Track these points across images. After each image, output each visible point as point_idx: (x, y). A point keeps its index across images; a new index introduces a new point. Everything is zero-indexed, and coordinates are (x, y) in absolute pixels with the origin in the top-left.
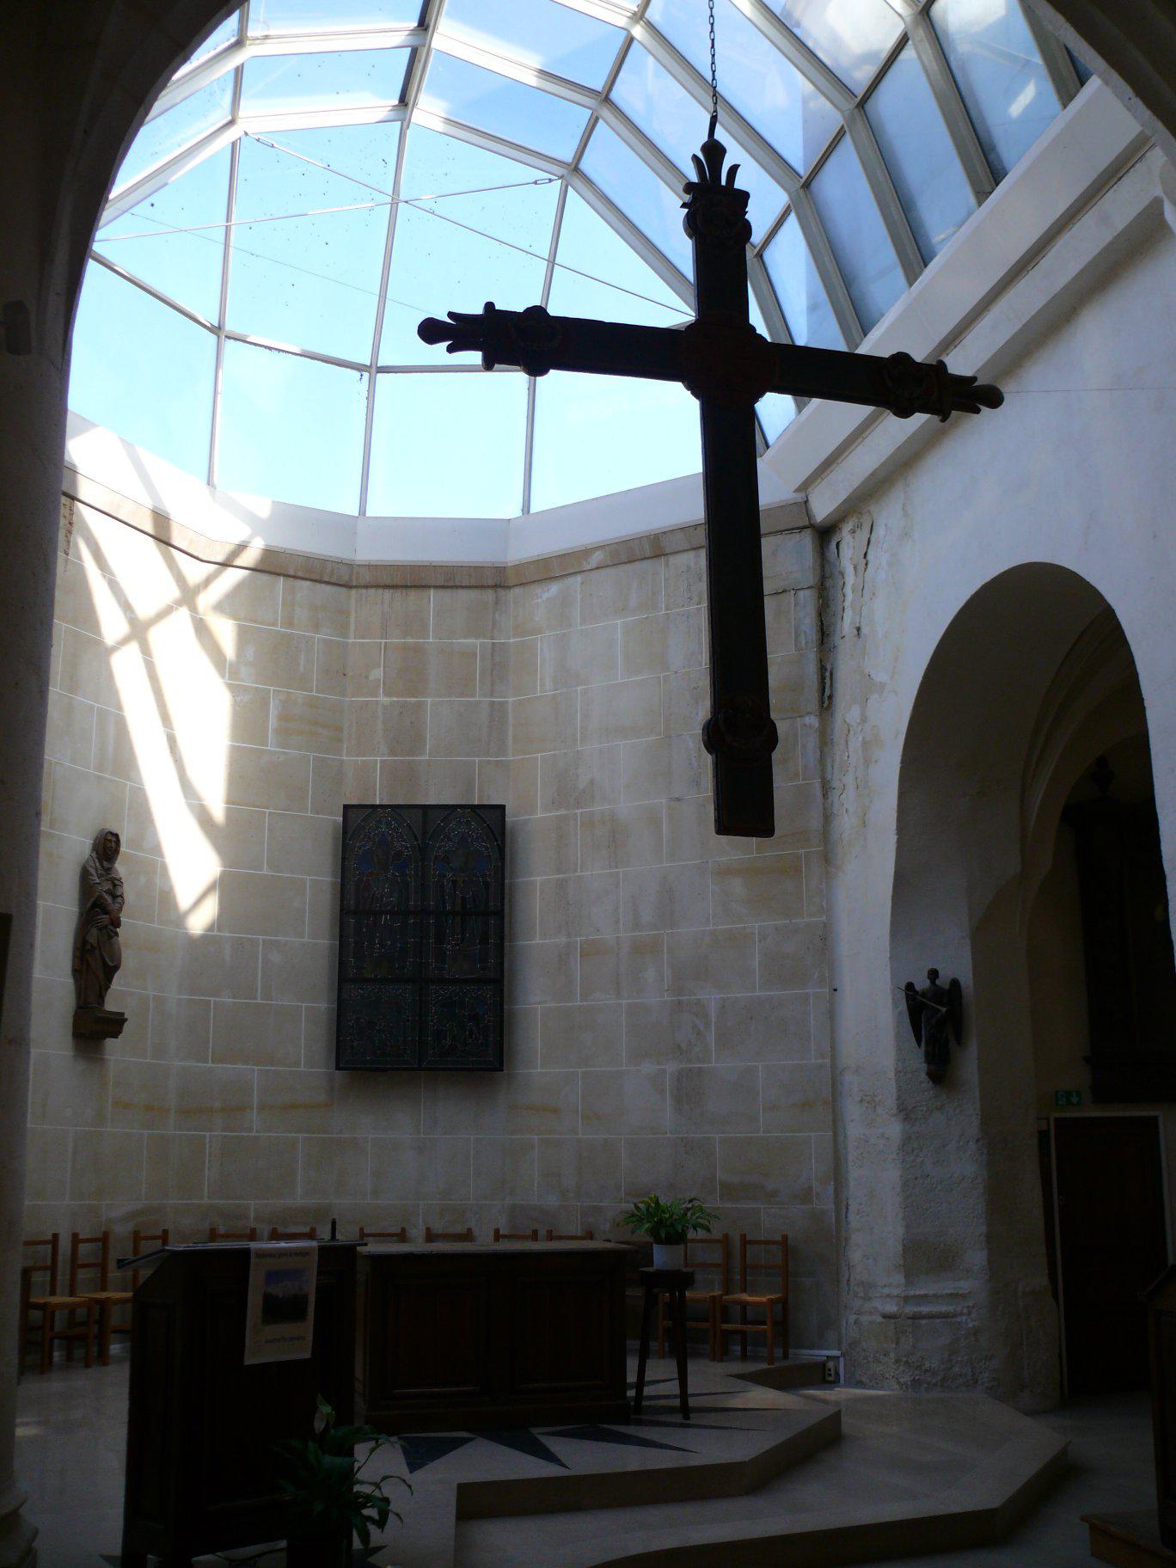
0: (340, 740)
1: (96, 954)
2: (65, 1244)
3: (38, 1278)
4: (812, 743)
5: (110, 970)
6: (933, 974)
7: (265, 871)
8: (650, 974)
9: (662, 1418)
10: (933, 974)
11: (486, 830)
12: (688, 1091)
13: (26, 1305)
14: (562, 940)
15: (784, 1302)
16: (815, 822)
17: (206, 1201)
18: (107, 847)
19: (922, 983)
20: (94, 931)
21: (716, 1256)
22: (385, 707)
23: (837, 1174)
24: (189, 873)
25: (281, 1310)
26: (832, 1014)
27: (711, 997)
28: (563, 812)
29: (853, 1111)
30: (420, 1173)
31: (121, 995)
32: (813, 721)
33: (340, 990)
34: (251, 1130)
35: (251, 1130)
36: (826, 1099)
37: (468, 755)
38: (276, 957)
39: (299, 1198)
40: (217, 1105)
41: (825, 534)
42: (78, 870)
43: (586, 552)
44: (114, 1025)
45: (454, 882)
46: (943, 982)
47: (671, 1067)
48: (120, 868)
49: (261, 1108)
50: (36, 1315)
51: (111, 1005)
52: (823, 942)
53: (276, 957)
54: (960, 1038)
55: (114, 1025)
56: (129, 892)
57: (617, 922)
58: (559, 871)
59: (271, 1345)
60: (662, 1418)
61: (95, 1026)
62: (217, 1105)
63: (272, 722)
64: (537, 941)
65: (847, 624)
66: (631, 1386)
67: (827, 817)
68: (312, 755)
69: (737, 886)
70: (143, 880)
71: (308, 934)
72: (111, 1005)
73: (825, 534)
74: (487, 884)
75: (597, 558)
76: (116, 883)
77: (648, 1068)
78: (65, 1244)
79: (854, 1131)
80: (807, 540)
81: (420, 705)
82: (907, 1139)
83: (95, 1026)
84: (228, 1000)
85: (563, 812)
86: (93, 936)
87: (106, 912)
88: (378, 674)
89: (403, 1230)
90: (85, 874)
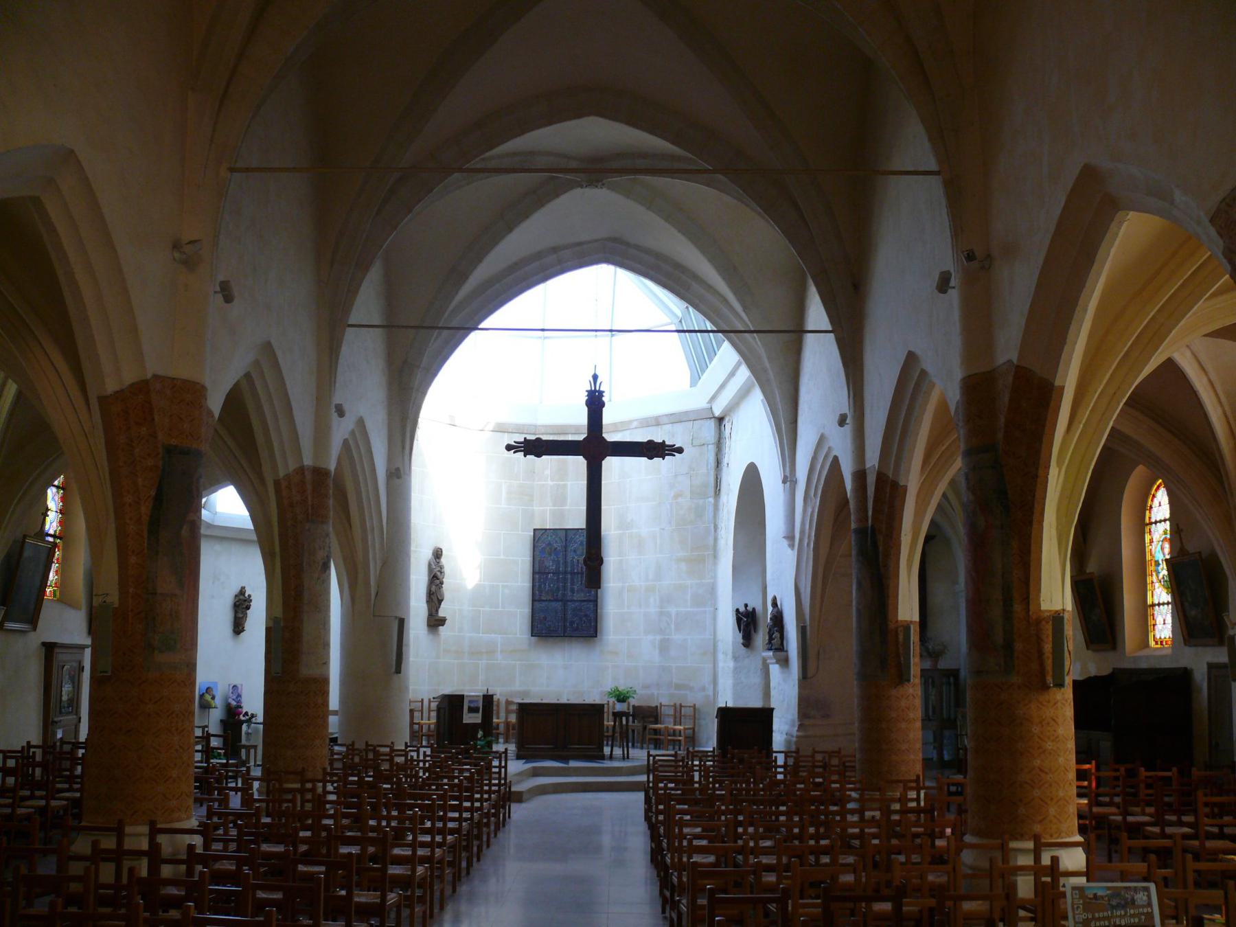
1: (434, 597)
2: (426, 703)
3: (417, 714)
4: (711, 508)
5: (440, 601)
6: (746, 606)
8: (652, 600)
10: (746, 606)
12: (664, 647)
13: (412, 723)
15: (693, 729)
16: (712, 542)
18: (438, 554)
19: (742, 609)
21: (672, 712)
23: (715, 682)
24: (468, 571)
25: (473, 710)
26: (715, 618)
27: (673, 610)
29: (721, 656)
30: (563, 676)
32: (712, 500)
36: (712, 651)
38: (507, 591)
39: (517, 687)
41: (720, 420)
43: (631, 422)
44: (442, 622)
46: (750, 608)
47: (658, 637)
48: (443, 560)
50: (416, 727)
51: (441, 614)
52: (712, 590)
53: (507, 591)
54: (756, 630)
55: (442, 622)
56: (447, 570)
59: (469, 718)
61: (435, 622)
65: (725, 461)
67: (716, 539)
69: (683, 566)
71: (520, 581)
72: (441, 614)
73: (720, 420)
75: (635, 424)
76: (441, 567)
77: (650, 637)
78: (426, 703)
79: (721, 664)
80: (712, 424)
81: (565, 486)
82: (735, 668)
83: (435, 622)
84: (487, 609)
86: (433, 588)
88: (548, 472)
90: (430, 565)
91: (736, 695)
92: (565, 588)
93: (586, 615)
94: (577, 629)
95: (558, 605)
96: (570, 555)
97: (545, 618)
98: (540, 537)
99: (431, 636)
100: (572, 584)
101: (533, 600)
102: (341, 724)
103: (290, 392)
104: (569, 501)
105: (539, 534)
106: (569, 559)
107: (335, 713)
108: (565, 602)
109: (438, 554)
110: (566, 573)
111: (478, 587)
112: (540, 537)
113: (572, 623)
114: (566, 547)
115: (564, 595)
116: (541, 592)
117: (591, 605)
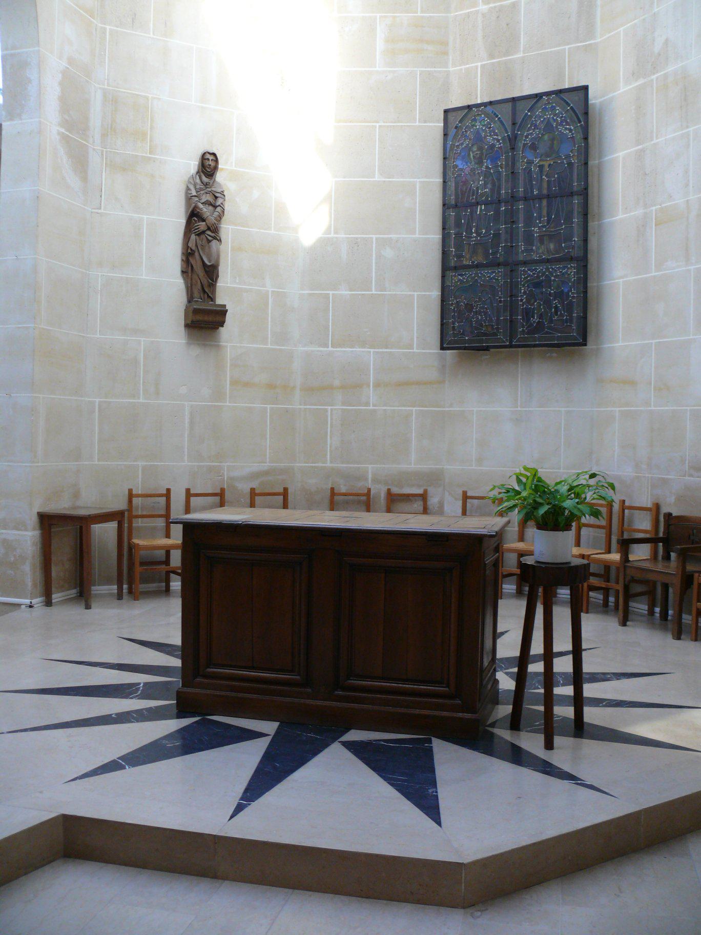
0: (446, 53)
7: (377, 178)
9: (141, 678)
11: (574, 108)
14: (639, 212)
17: (328, 464)
18: (208, 166)
20: (193, 237)
22: (484, 15)
28: (641, 81)
31: (227, 289)
33: (443, 277)
34: (367, 404)
35: (367, 404)
37: (559, 45)
38: (388, 253)
40: (337, 383)
42: (184, 187)
45: (541, 167)
49: (377, 385)
53: (388, 253)
57: (687, 185)
58: (638, 142)
60: (141, 678)
62: (337, 383)
63: (380, 45)
64: (621, 216)
66: (536, 659)
68: (418, 70)
70: (256, 194)
71: (418, 231)
74: (570, 165)
85: (641, 81)
87: (204, 220)
89: (426, 491)
91: (438, 121)
92: (512, 234)
93: (560, 295)
94: (539, 327)
95: (497, 275)
96: (525, 157)
97: (469, 307)
98: (458, 121)
99: (196, 351)
100: (529, 221)
101: (445, 268)
102: (184, 559)
103: (439, 180)
104: (523, 41)
105: (454, 119)
106: (521, 166)
107: (562, 603)
108: (512, 266)
109: (208, 166)
110: (514, 198)
111: (323, 242)
112: (458, 121)
113: (528, 314)
114: (513, 140)
115: (510, 249)
116: (459, 246)
117: (572, 271)
